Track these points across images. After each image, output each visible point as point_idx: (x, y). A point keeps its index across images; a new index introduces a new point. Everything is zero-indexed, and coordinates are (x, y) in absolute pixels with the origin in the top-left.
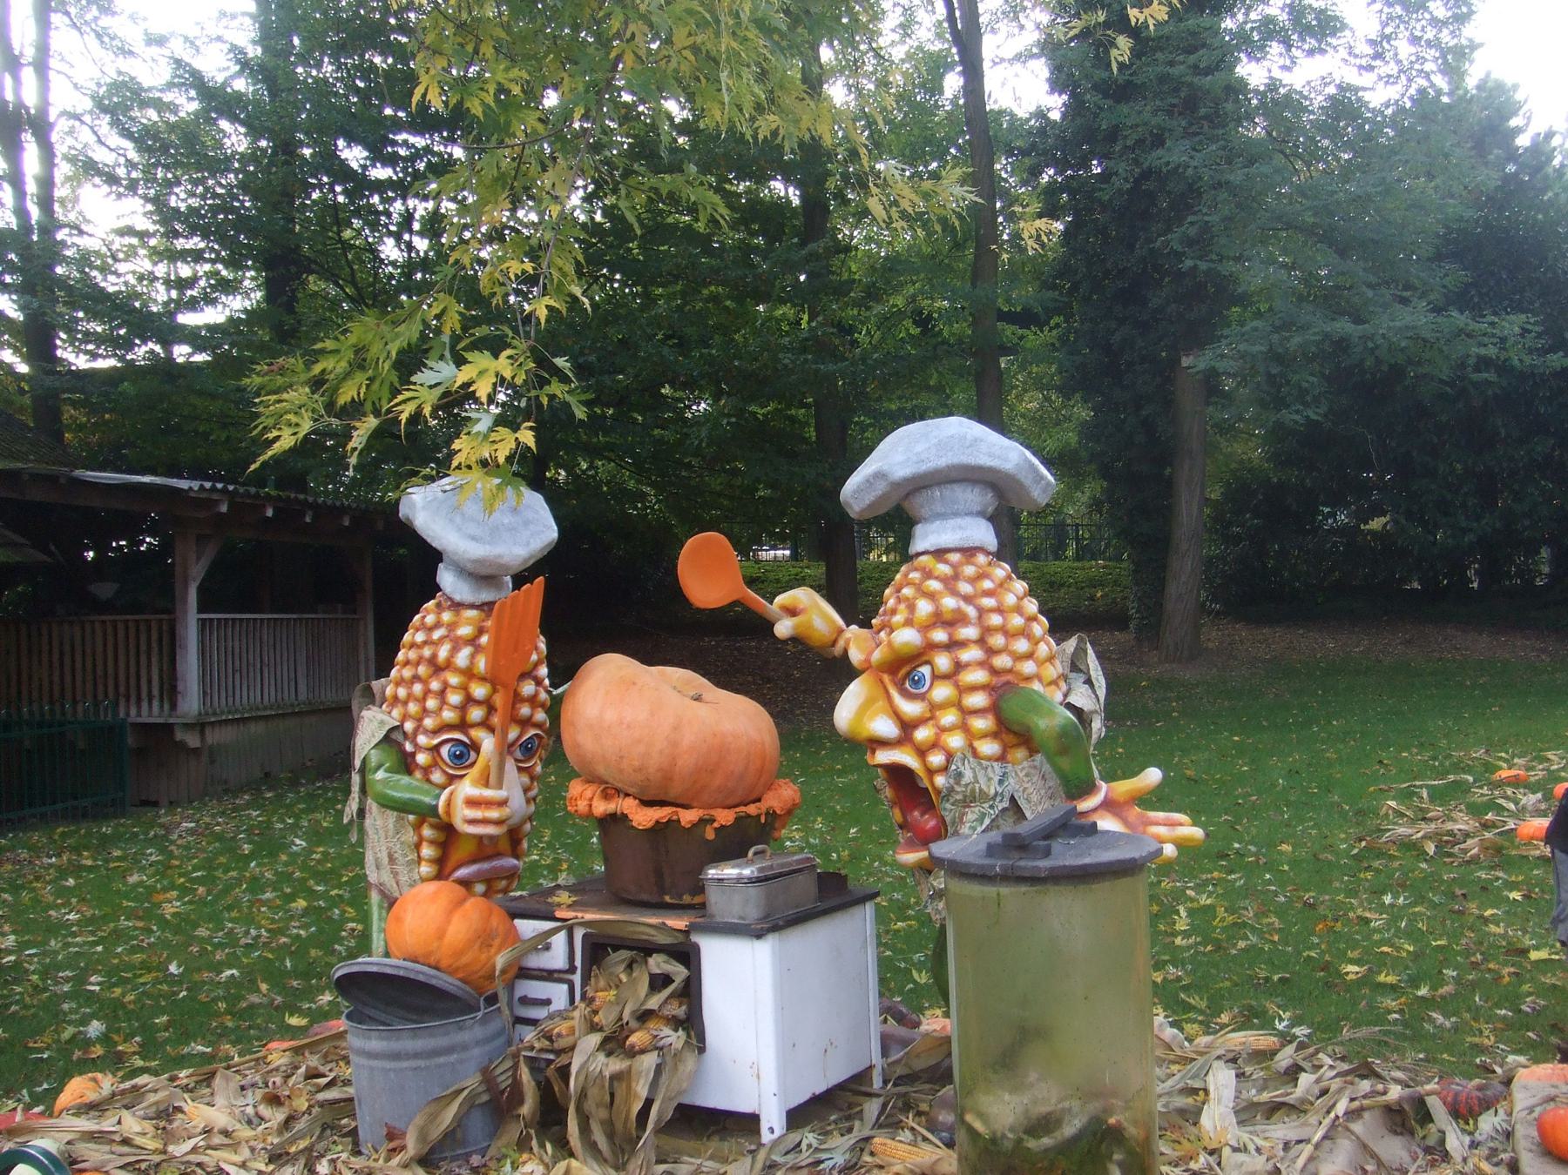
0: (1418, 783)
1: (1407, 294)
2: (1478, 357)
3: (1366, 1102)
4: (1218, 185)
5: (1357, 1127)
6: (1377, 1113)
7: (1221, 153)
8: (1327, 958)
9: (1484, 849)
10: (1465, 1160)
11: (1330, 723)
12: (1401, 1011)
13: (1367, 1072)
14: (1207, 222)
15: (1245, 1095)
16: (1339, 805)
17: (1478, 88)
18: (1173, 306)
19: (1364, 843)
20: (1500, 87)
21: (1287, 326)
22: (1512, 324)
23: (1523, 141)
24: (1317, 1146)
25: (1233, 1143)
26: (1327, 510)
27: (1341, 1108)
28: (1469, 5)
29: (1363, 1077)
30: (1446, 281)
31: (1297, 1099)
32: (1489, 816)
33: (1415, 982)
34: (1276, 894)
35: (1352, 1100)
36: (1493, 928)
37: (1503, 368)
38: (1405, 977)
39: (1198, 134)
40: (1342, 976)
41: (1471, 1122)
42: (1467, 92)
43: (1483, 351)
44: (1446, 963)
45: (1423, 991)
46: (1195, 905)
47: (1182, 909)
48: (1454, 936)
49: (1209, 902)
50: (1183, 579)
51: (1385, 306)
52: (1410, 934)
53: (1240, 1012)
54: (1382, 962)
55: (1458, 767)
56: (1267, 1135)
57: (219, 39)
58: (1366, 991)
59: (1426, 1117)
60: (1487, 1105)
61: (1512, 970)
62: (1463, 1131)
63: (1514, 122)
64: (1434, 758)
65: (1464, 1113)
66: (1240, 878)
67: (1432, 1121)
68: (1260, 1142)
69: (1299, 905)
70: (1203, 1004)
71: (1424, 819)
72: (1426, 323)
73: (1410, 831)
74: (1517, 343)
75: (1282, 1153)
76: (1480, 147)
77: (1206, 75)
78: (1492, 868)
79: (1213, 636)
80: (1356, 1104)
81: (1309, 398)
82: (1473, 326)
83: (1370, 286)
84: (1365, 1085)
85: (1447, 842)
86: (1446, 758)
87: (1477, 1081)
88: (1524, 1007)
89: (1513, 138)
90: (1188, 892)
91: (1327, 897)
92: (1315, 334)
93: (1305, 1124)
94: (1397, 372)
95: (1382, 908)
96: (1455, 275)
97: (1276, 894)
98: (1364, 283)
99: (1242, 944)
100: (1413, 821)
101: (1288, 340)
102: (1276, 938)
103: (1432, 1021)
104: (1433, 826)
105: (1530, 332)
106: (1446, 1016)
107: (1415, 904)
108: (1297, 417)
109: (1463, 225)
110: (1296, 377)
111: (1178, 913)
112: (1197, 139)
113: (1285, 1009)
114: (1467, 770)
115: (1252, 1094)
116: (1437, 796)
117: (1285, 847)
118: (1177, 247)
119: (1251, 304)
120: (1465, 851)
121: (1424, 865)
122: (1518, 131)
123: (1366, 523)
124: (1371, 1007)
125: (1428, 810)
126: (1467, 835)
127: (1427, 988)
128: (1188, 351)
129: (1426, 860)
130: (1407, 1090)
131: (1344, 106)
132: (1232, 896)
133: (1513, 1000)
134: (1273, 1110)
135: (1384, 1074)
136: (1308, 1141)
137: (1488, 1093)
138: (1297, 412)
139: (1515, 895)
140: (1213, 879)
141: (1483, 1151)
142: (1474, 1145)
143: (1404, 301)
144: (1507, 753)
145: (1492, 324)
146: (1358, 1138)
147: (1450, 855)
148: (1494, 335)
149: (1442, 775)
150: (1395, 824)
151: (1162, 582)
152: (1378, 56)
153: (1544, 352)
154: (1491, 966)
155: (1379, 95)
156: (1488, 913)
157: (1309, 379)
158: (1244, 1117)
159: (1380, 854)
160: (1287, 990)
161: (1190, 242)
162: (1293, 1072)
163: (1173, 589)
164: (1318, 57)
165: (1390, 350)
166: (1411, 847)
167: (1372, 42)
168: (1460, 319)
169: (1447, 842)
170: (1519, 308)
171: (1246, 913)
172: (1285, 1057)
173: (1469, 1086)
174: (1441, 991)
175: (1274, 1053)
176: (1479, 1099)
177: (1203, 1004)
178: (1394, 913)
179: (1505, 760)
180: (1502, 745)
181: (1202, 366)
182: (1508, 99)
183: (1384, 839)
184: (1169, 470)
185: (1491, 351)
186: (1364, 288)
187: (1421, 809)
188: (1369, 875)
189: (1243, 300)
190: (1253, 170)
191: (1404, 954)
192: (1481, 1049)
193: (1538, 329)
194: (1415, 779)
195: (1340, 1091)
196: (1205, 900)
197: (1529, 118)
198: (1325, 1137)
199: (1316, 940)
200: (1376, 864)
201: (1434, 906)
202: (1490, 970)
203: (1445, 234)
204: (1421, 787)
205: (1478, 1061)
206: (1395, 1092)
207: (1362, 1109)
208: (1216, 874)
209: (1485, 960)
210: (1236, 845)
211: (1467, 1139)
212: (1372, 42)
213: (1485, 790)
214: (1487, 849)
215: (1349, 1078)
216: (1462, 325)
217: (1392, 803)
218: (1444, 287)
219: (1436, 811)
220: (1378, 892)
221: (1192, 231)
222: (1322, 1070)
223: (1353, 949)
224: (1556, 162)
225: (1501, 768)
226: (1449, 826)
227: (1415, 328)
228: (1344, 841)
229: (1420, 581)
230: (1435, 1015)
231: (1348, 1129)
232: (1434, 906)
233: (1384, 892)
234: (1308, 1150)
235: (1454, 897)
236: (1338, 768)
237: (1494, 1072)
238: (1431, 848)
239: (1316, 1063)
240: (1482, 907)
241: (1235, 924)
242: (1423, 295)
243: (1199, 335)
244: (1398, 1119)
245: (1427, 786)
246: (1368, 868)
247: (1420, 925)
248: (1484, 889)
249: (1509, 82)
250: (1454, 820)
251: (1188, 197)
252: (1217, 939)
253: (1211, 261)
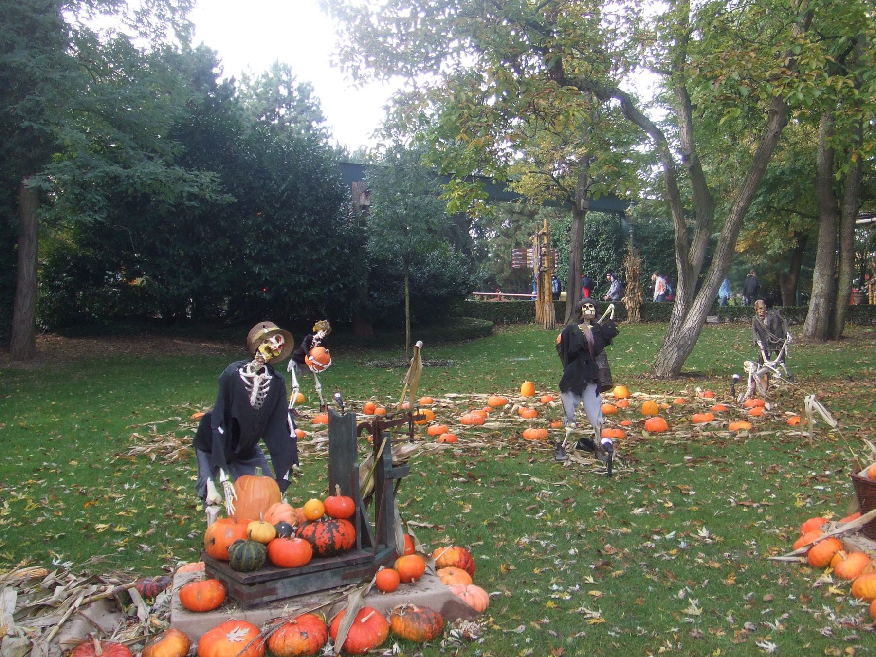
0: (152, 423)
1: (152, 155)
2: (189, 192)
3: (93, 597)
4: (47, 80)
5: (87, 612)
6: (100, 603)
8: (88, 521)
9: (181, 455)
10: (146, 620)
11: (108, 392)
12: (125, 546)
13: (95, 580)
14: (38, 101)
15: (22, 604)
16: (108, 437)
17: (198, 49)
18: (19, 148)
19: (118, 457)
20: (208, 50)
21: (84, 166)
22: (206, 177)
23: (219, 81)
24: (61, 627)
25: (11, 633)
26: (110, 273)
27: (77, 603)
28: (190, 3)
29: (93, 584)
30: (175, 151)
31: (52, 602)
32: (186, 438)
33: (135, 530)
34: (64, 489)
35: (85, 597)
36: (180, 496)
37: (203, 200)
38: (130, 527)
39: (34, 47)
40: (94, 530)
41: (153, 599)
42: (191, 50)
43: (191, 190)
44: (153, 517)
45: (139, 534)
46: (15, 500)
48: (159, 502)
49: (24, 497)
50: (24, 311)
51: (140, 160)
52: (136, 504)
53: (33, 558)
54: (119, 520)
55: (175, 413)
56: (33, 625)
57: (349, 86)
58: (108, 537)
59: (129, 601)
60: (161, 589)
61: (187, 517)
63: (215, 70)
64: (163, 409)
65: (148, 595)
66: (45, 482)
67: (133, 602)
68: (26, 629)
69: (77, 494)
70: (11, 557)
71: (153, 442)
72: (162, 172)
73: (144, 449)
74: (208, 187)
76: (197, 81)
77: (41, 13)
78: (185, 465)
79: (42, 341)
80: (88, 599)
81: (96, 208)
82: (187, 176)
83: (133, 149)
84: (94, 588)
85: (162, 453)
86: (168, 408)
87: (157, 577)
88: (190, 536)
89: (214, 79)
90: (12, 493)
91: (94, 488)
92: (100, 172)
93: (56, 615)
94: (146, 197)
95: (124, 491)
96: (179, 148)
97: (64, 489)
98: (130, 146)
99: (40, 519)
100: (147, 443)
101: (85, 173)
102: (60, 514)
103: (141, 549)
104: (157, 445)
105: (215, 181)
106: (149, 545)
107: (140, 488)
108: (89, 219)
109: (184, 121)
110: (90, 196)
111: (3, 506)
112: (33, 50)
113: (59, 553)
114: (179, 414)
115: (27, 603)
116: (162, 429)
117: (74, 463)
118: (19, 112)
119: (66, 152)
120: (171, 457)
121: (149, 466)
122: (217, 75)
123: (131, 281)
124: (109, 545)
125: (155, 437)
126: (174, 448)
127: (141, 531)
128: (28, 176)
129: (150, 464)
130: (118, 587)
131: (123, 47)
132: (37, 492)
133: (185, 532)
134: (38, 610)
135: (106, 580)
136: (56, 624)
137: (162, 582)
138: (90, 216)
139: (194, 478)
140: (28, 484)
142: (152, 611)
143: (150, 158)
144: (200, 404)
145: (196, 176)
146: (87, 618)
147: (163, 460)
148: (197, 182)
149: (165, 417)
150: (137, 445)
151: (12, 312)
152: (140, 21)
153: (222, 192)
154: (176, 516)
155: (142, 44)
156: (180, 488)
157: (97, 198)
158: (19, 617)
159: (127, 462)
160: (64, 543)
161: (30, 111)
162: (52, 589)
163: (18, 316)
164: (108, 16)
165: (142, 184)
166: (144, 457)
167: (136, 13)
168: (179, 171)
169: (163, 453)
170: (209, 169)
171: (44, 501)
172: (48, 581)
173: (152, 581)
174: (148, 532)
175: (43, 578)
176: (157, 586)
177: (11, 557)
178: (129, 493)
179: (199, 408)
180: (199, 400)
181: (33, 185)
182: (212, 58)
183: (129, 454)
184: (16, 245)
185: (195, 190)
186: (129, 150)
188: (119, 474)
189: (60, 148)
190: (67, 73)
191: (131, 515)
192: (164, 560)
193: (219, 180)
194: (151, 421)
195: (78, 593)
196: (21, 497)
197: (222, 70)
198: (66, 621)
199: (83, 512)
200: (124, 468)
201: (152, 487)
203: (175, 125)
204: (153, 424)
205: (162, 567)
206: (111, 589)
207: (91, 601)
208: (30, 481)
209: (174, 513)
210: (45, 464)
211: (149, 609)
212: (136, 13)
213: (186, 424)
214: (183, 455)
215: (84, 586)
216: (180, 174)
217: (136, 434)
218: (173, 153)
219: (160, 437)
220: (122, 483)
221: (29, 105)
222: (69, 584)
223: (104, 515)
224: (236, 95)
225: (196, 412)
226: (165, 444)
227: (156, 174)
228: (108, 457)
229: (161, 313)
230: (143, 546)
231: (81, 614)
232: (152, 487)
233: (125, 483)
234: (56, 628)
235: (162, 482)
236: (111, 417)
237: (170, 571)
238: (154, 457)
239: (67, 580)
240: (177, 485)
241: (38, 508)
242: (161, 156)
243: (34, 167)
244: (113, 604)
245: (157, 424)
246: (119, 470)
247: (142, 498)
248: (179, 476)
249: (213, 49)
250: (169, 441)
251: (29, 84)
252: (26, 518)
253: (40, 123)
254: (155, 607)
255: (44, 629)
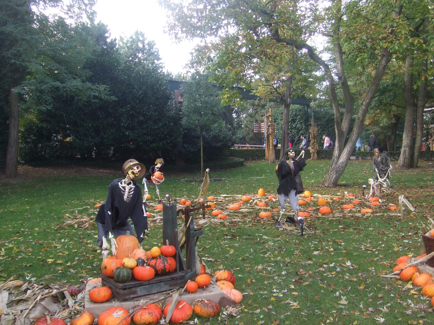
0: (75, 209)
1: (75, 77)
2: (93, 95)
3: (46, 295)
4: (23, 39)
5: (43, 303)
6: (49, 298)
7: (24, 30)
8: (44, 258)
9: (90, 225)
10: (72, 307)
11: (54, 194)
12: (62, 270)
13: (47, 287)
14: (19, 50)
15: (11, 299)
16: (53, 216)
17: (98, 24)
18: (10, 73)
19: (58, 226)
20: (103, 25)
21: (42, 82)
22: (102, 87)
23: (109, 40)
24: (30, 310)
25: (6, 313)
26: (55, 135)
27: (38, 299)
28: (94, 1)
29: (46, 289)
31: (26, 298)
32: (92, 217)
33: (67, 262)
34: (32, 242)
35: (42, 295)
36: (89, 245)
37: (100, 99)
38: (65, 261)
39: (17, 23)
40: (47, 262)
41: (76, 296)
42: (95, 25)
43: (95, 94)
45: (69, 264)
46: (7, 247)
47: (3, 250)
48: (79, 249)
49: (12, 246)
51: (70, 79)
52: (67, 249)
53: (16, 276)
54: (59, 257)
55: (87, 204)
56: (16, 309)
58: (53, 266)
59: (64, 297)
61: (92, 256)
62: (73, 299)
63: (107, 35)
64: (81, 202)
65: (73, 294)
66: (22, 239)
67: (66, 298)
68: (13, 311)
69: (38, 244)
70: (6, 275)
71: (76, 218)
73: (71, 222)
74: (103, 92)
75: (20, 313)
76: (98, 40)
77: (20, 7)
78: (92, 230)
79: (21, 169)
80: (43, 296)
81: (48, 103)
82: (92, 87)
83: (66, 74)
84: (47, 291)
85: (80, 224)
86: (83, 202)
87: (78, 285)
88: (94, 265)
89: (106, 39)
90: (6, 244)
91: (46, 241)
92: (50, 85)
93: (28, 304)
94: (72, 98)
95: (61, 243)
96: (89, 73)
97: (32, 242)
98: (64, 72)
99: (20, 257)
100: (73, 219)
101: (42, 86)
102: (30, 254)
103: (70, 271)
104: (78, 220)
105: (106, 90)
106: (74, 269)
107: (69, 241)
108: (44, 108)
109: (91, 60)
110: (44, 97)
111: (1, 250)
112: (16, 25)
113: (29, 273)
114: (89, 205)
115: (14, 298)
116: (80, 212)
117: (37, 229)
118: (9, 55)
119: (33, 75)
120: (85, 226)
121: (74, 231)
122: (107, 37)
123: (65, 139)
124: (54, 270)
125: (77, 216)
126: (86, 222)
127: (70, 263)
128: (14, 87)
129: (74, 229)
130: (58, 290)
131: (61, 23)
132: (18, 243)
133: (92, 263)
134: (19, 302)
135: (52, 287)
136: (28, 309)
137: (80, 288)
138: (44, 107)
139: (96, 236)
140: (14, 239)
141: (78, 303)
142: (75, 302)
143: (75, 78)
144: (99, 200)
145: (97, 87)
146: (43, 306)
147: (81, 227)
148: (98, 90)
149: (82, 206)
150: (68, 220)
151: (6, 154)
152: (69, 10)
153: (110, 95)
154: (87, 255)
155: (70, 22)
156: (89, 241)
157: (48, 98)
158: (9, 305)
159: (63, 229)
160: (31, 268)
161: (15, 55)
162: (26, 291)
163: (9, 156)
164: (54, 8)
165: (70, 91)
166: (71, 226)
167: (68, 6)
168: (89, 85)
169: (81, 224)
170: (103, 84)
171: (22, 248)
172: (24, 287)
173: (76, 287)
174: (73, 263)
175: (21, 286)
176: (78, 290)
177: (6, 275)
178: (64, 244)
179: (98, 202)
180: (98, 198)
181: (16, 91)
182: (105, 29)
183: (64, 225)
184: (8, 121)
185: (97, 94)
186: (64, 74)
187: (75, 216)
188: (59, 235)
189: (30, 73)
190: (33, 36)
191: (65, 255)
192: (81, 277)
193: (109, 89)
194: (75, 208)
195: (39, 293)
196: (11, 246)
197: (110, 35)
198: (33, 307)
199: (41, 253)
200: (61, 231)
201: (75, 241)
202: (87, 256)
203: (87, 62)
204: (76, 210)
205: (80, 280)
206: (55, 291)
207: (45, 298)
208: (15, 238)
209: (86, 254)
210: (22, 229)
211: (74, 301)
212: (68, 6)
213: (92, 210)
214: (91, 225)
215: (42, 290)
216: (89, 86)
217: (67, 215)
218: (86, 76)
219: (79, 216)
220: (61, 239)
221: (14, 52)
222: (34, 289)
223: (52, 255)
224: (117, 47)
225: (97, 204)
226: (82, 220)
227: (77, 86)
228: (53, 226)
229: (80, 155)
230: (71, 270)
231: (40, 304)
232: (75, 241)
233: (62, 239)
234: (28, 311)
235: (80, 238)
236: (55, 206)
237: (84, 283)
238: (76, 226)
239: (33, 287)
240: (88, 240)
241: (19, 252)
242: (80, 77)
243: (17, 82)
244: (56, 299)
245: (78, 210)
246: (59, 233)
247: (70, 247)
248: (89, 235)
249: (105, 24)
250: (84, 218)
251: (14, 42)
253: (20, 61)
254: (77, 300)
255: (22, 311)
